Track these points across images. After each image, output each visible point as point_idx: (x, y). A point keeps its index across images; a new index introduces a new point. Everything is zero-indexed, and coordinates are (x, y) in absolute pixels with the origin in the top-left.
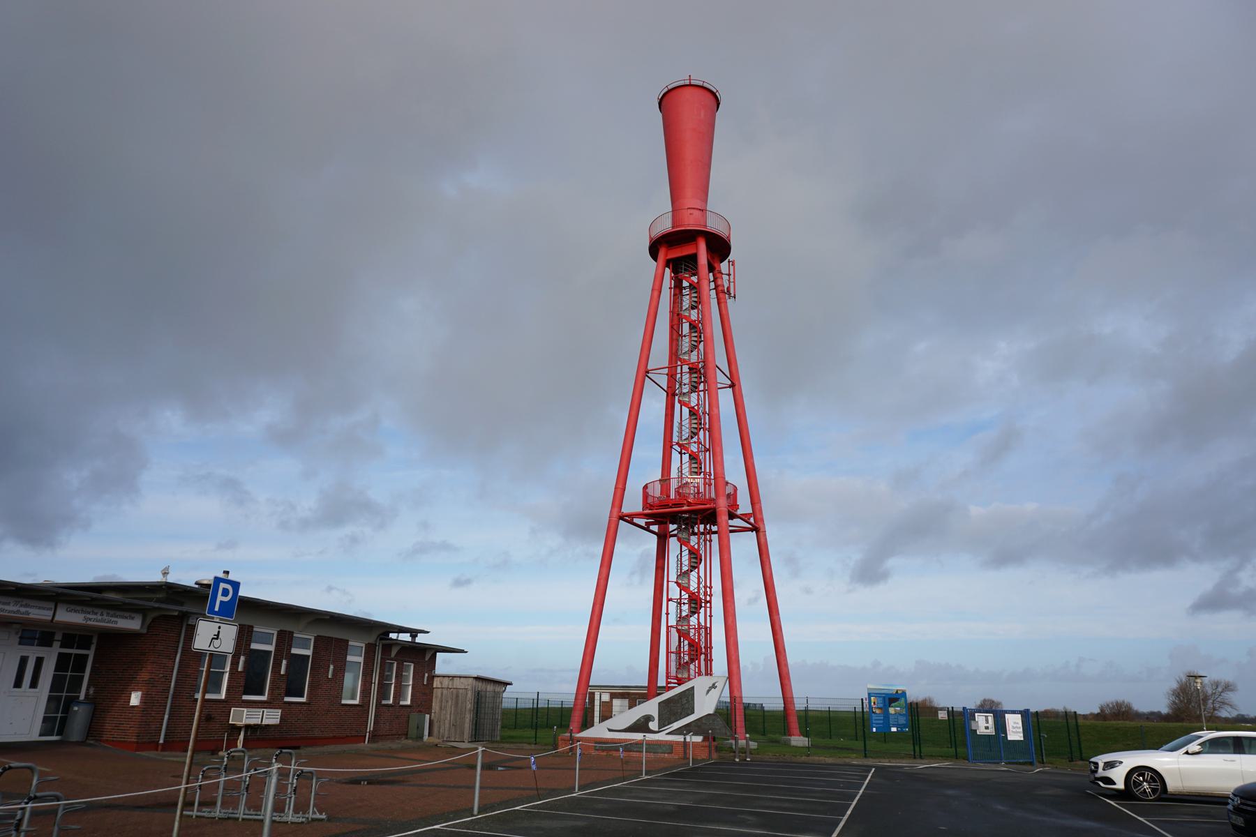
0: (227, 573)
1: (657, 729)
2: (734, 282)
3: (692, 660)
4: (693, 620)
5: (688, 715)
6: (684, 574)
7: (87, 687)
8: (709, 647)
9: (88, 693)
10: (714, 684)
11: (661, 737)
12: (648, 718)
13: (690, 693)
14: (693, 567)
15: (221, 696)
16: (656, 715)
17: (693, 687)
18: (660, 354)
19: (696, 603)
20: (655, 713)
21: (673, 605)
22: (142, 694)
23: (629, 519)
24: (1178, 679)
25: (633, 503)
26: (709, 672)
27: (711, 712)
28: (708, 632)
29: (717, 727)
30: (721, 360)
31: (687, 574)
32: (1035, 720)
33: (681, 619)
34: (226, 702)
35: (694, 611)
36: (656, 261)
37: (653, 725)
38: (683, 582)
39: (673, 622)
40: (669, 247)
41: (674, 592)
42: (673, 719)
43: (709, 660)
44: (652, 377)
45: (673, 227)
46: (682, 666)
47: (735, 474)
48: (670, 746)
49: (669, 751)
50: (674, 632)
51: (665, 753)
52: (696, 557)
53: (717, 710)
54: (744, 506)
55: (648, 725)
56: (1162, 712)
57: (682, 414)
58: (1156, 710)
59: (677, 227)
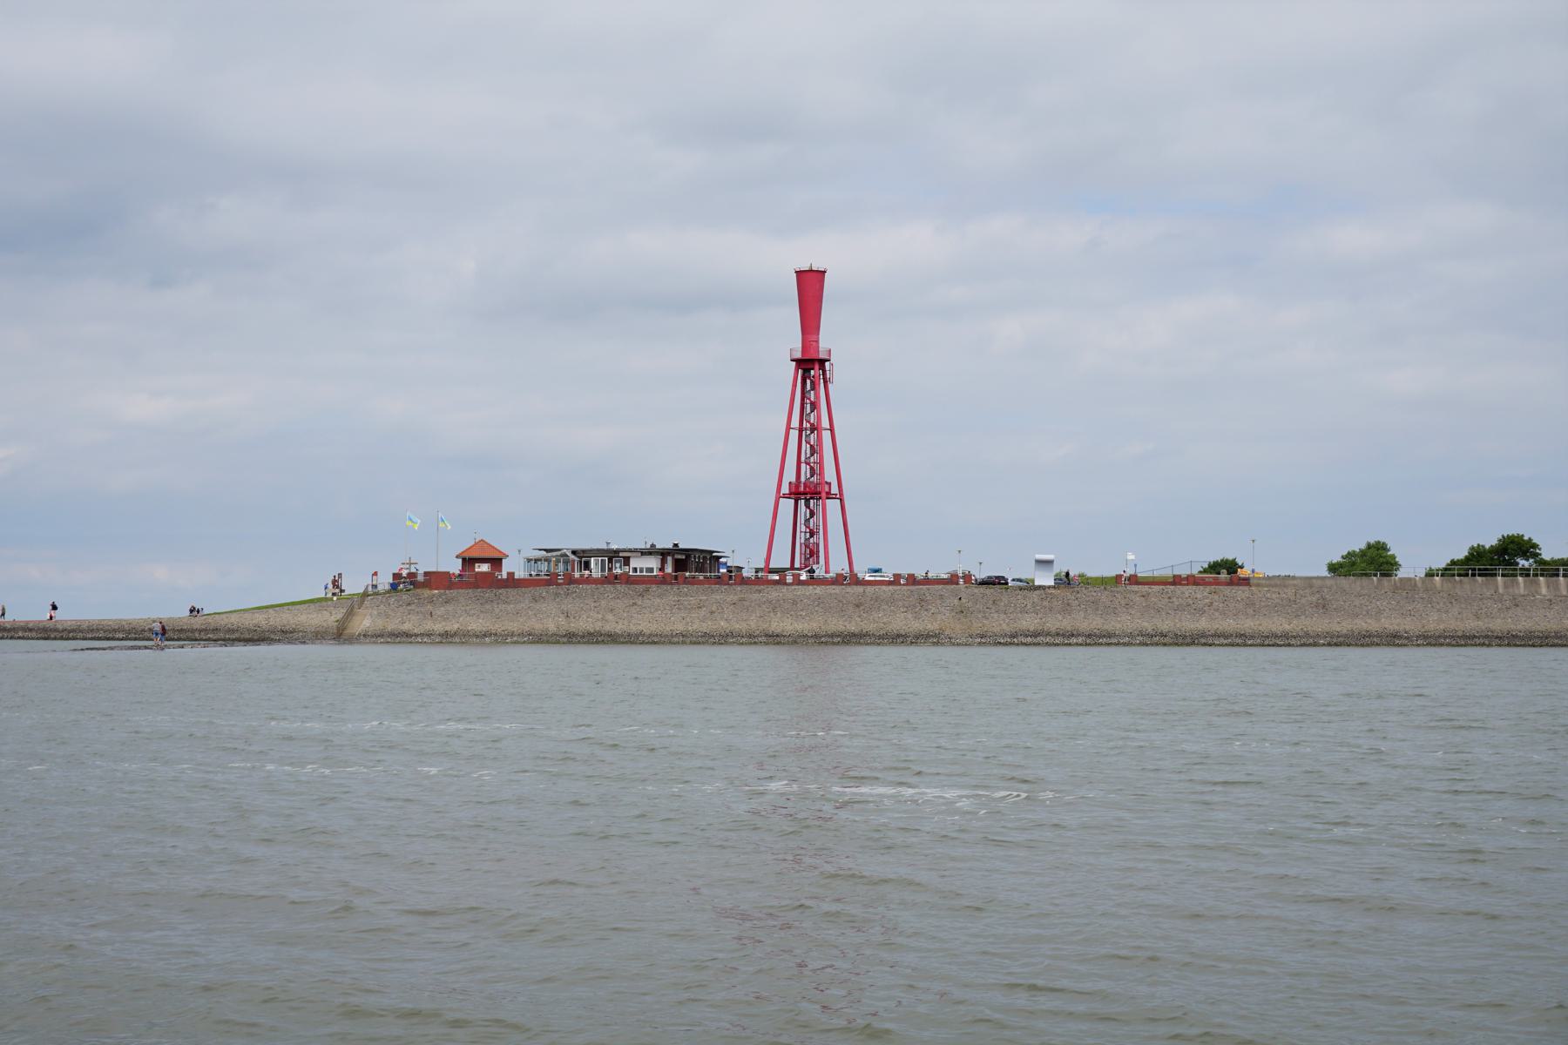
0: (676, 545)
2: (832, 430)
3: (811, 557)
4: (811, 540)
6: (807, 521)
8: (818, 552)
14: (812, 455)
18: (795, 423)
19: (812, 534)
21: (803, 534)
23: (785, 496)
25: (785, 490)
26: (818, 563)
28: (818, 545)
30: (825, 423)
31: (809, 458)
33: (806, 540)
35: (812, 535)
38: (808, 461)
39: (803, 541)
41: (803, 528)
43: (818, 557)
46: (806, 559)
47: (830, 475)
50: (803, 546)
52: (812, 514)
54: (835, 490)
56: (1494, 544)
57: (805, 448)
58: (1219, 559)
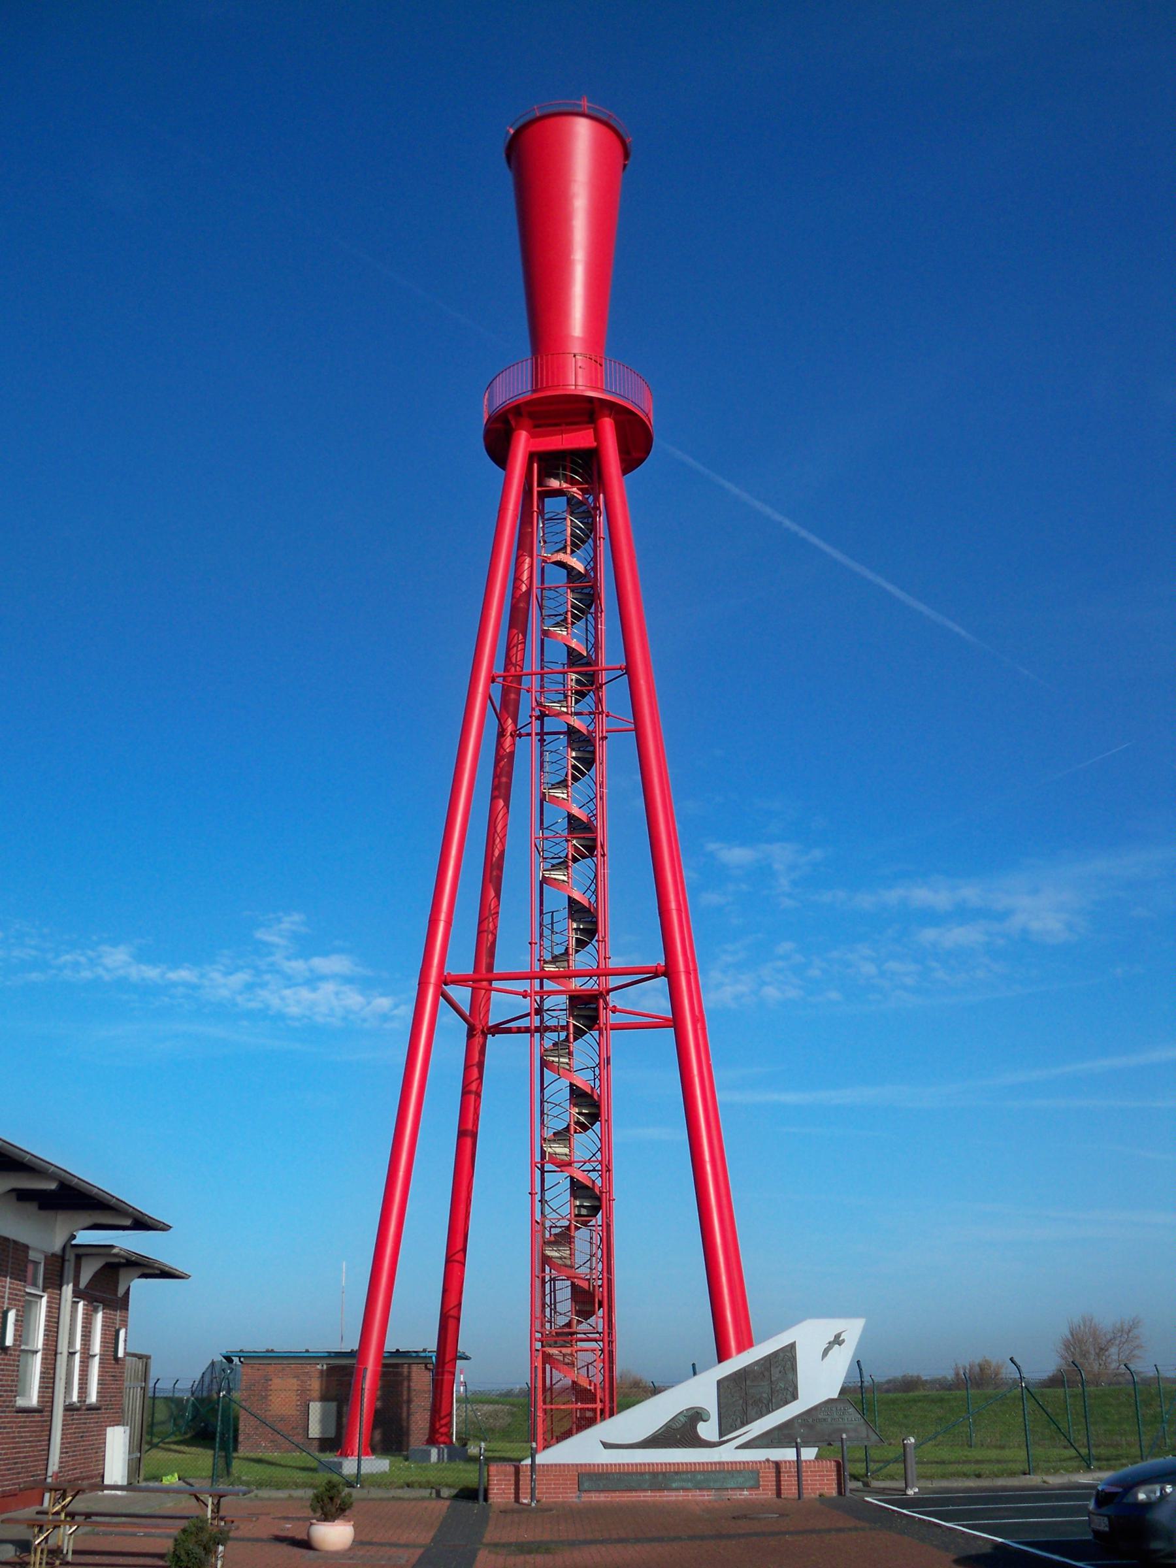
1: (714, 1437)
5: (786, 1403)
7: (496, 941)
9: (554, 1241)
10: (838, 1336)
11: (727, 1454)
12: (696, 1415)
13: (790, 1354)
15: (30, 1398)
16: (712, 1407)
17: (792, 1346)
20: (710, 1404)
22: (866, 1321)
24: (1070, 1320)
27: (835, 1395)
29: (849, 1426)
32: (152, 1402)
34: (98, 1409)
36: (504, 469)
37: (708, 1430)
40: (536, 426)
42: (752, 1412)
44: (522, 726)
45: (534, 391)
48: (751, 1472)
49: (752, 1483)
51: (742, 1489)
53: (843, 1391)
55: (696, 1432)
59: (542, 389)
